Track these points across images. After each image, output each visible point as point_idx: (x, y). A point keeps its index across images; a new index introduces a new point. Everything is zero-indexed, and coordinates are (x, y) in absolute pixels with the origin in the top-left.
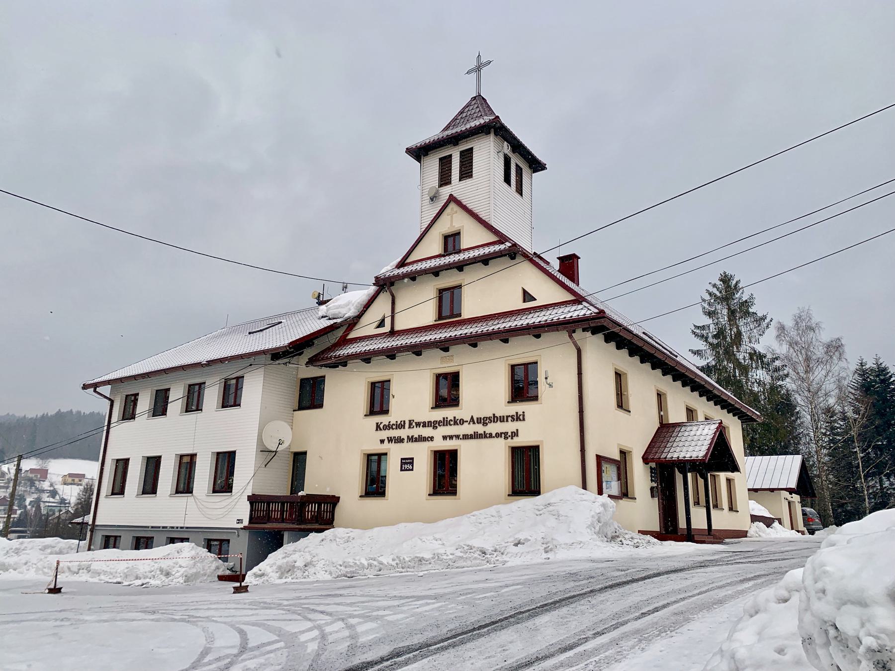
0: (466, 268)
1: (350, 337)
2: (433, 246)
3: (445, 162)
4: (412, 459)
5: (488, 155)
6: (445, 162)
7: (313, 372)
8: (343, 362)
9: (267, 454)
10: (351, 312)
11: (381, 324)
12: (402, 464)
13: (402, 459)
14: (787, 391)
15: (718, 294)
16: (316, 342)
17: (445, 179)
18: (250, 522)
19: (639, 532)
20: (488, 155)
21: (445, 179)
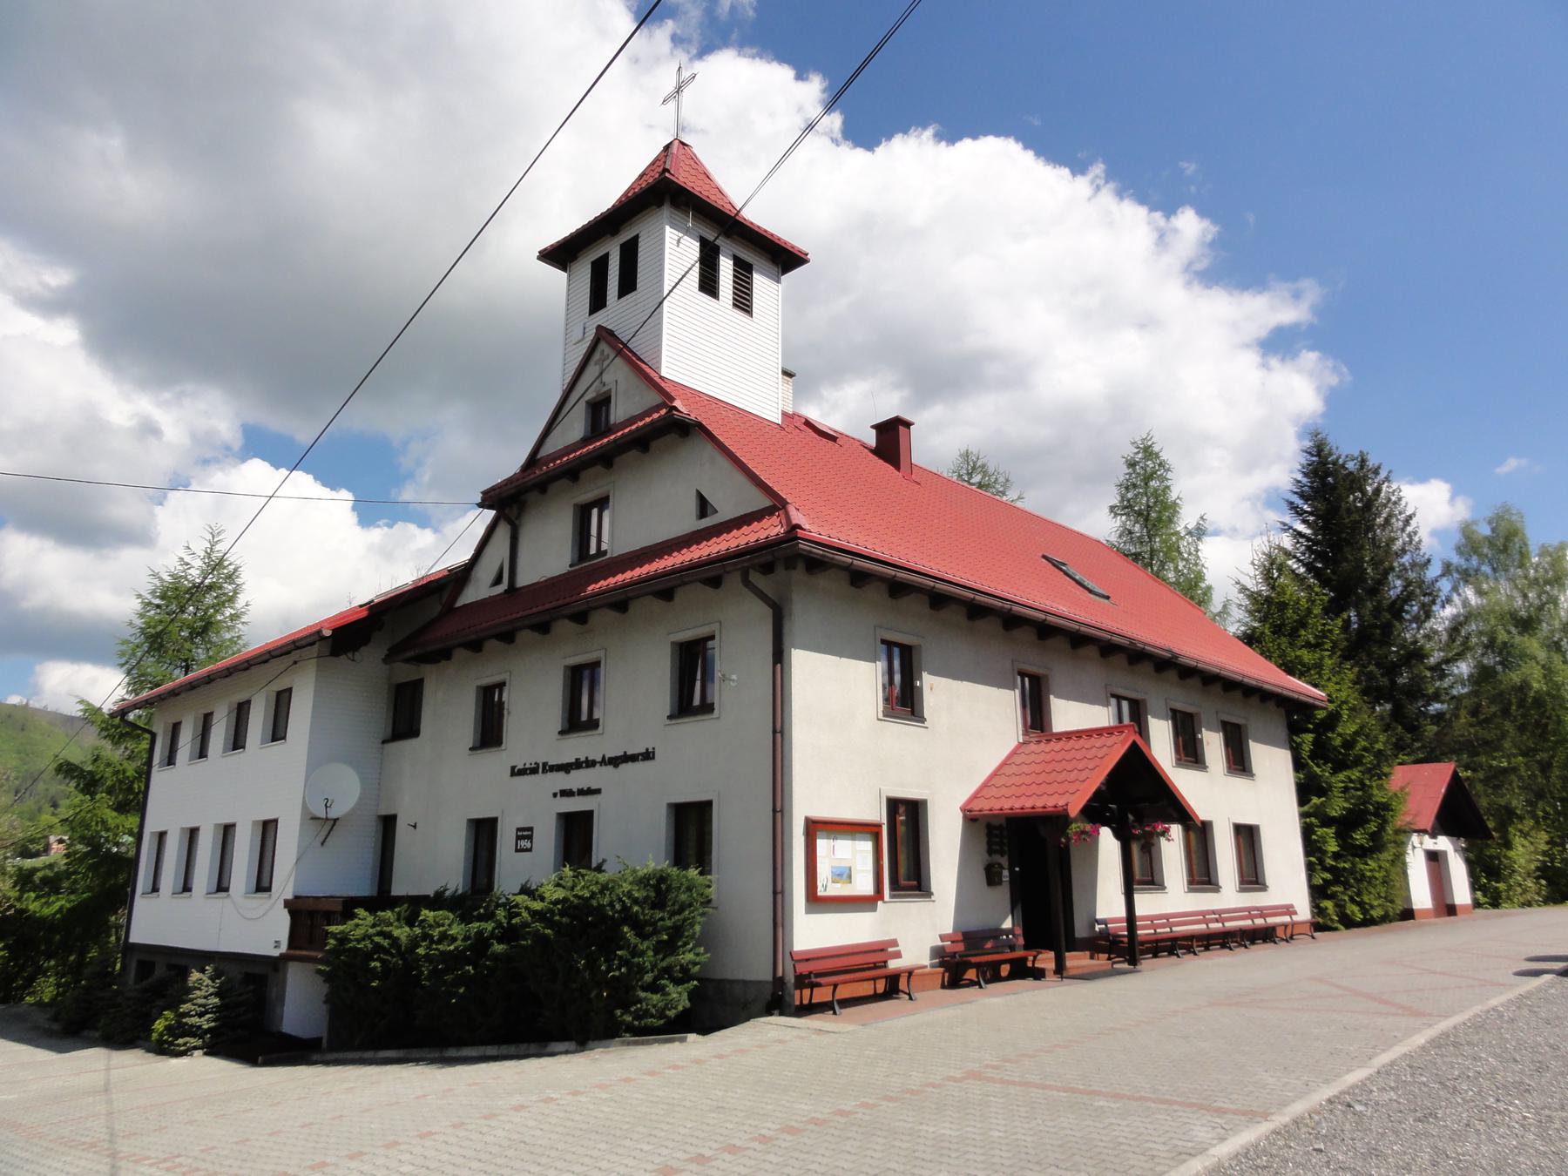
0: (584, 475)
1: (461, 602)
2: (574, 428)
3: (600, 269)
4: (531, 829)
5: (676, 249)
6: (600, 269)
7: (405, 673)
8: (442, 655)
9: (324, 826)
10: (462, 555)
11: (498, 581)
12: (518, 838)
13: (519, 830)
14: (1386, 775)
15: (1308, 531)
16: (596, 716)
17: (598, 301)
18: (291, 945)
19: (598, 791)
20: (676, 249)
21: (598, 301)
